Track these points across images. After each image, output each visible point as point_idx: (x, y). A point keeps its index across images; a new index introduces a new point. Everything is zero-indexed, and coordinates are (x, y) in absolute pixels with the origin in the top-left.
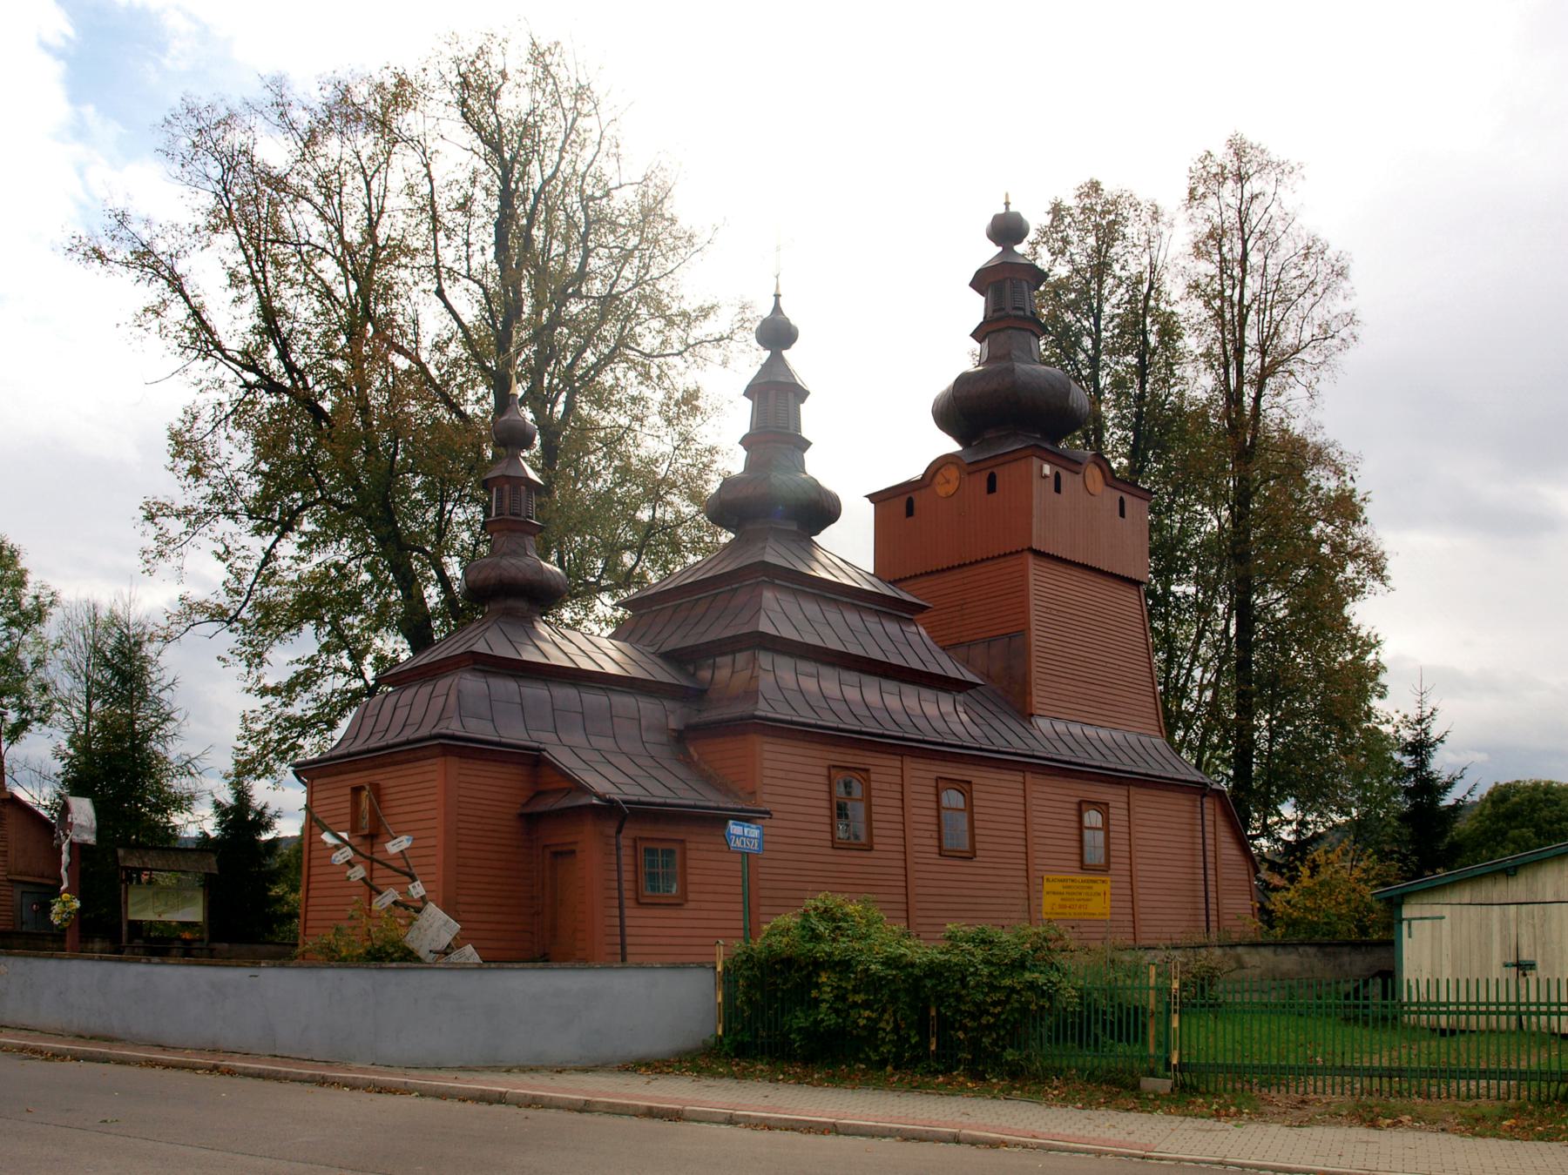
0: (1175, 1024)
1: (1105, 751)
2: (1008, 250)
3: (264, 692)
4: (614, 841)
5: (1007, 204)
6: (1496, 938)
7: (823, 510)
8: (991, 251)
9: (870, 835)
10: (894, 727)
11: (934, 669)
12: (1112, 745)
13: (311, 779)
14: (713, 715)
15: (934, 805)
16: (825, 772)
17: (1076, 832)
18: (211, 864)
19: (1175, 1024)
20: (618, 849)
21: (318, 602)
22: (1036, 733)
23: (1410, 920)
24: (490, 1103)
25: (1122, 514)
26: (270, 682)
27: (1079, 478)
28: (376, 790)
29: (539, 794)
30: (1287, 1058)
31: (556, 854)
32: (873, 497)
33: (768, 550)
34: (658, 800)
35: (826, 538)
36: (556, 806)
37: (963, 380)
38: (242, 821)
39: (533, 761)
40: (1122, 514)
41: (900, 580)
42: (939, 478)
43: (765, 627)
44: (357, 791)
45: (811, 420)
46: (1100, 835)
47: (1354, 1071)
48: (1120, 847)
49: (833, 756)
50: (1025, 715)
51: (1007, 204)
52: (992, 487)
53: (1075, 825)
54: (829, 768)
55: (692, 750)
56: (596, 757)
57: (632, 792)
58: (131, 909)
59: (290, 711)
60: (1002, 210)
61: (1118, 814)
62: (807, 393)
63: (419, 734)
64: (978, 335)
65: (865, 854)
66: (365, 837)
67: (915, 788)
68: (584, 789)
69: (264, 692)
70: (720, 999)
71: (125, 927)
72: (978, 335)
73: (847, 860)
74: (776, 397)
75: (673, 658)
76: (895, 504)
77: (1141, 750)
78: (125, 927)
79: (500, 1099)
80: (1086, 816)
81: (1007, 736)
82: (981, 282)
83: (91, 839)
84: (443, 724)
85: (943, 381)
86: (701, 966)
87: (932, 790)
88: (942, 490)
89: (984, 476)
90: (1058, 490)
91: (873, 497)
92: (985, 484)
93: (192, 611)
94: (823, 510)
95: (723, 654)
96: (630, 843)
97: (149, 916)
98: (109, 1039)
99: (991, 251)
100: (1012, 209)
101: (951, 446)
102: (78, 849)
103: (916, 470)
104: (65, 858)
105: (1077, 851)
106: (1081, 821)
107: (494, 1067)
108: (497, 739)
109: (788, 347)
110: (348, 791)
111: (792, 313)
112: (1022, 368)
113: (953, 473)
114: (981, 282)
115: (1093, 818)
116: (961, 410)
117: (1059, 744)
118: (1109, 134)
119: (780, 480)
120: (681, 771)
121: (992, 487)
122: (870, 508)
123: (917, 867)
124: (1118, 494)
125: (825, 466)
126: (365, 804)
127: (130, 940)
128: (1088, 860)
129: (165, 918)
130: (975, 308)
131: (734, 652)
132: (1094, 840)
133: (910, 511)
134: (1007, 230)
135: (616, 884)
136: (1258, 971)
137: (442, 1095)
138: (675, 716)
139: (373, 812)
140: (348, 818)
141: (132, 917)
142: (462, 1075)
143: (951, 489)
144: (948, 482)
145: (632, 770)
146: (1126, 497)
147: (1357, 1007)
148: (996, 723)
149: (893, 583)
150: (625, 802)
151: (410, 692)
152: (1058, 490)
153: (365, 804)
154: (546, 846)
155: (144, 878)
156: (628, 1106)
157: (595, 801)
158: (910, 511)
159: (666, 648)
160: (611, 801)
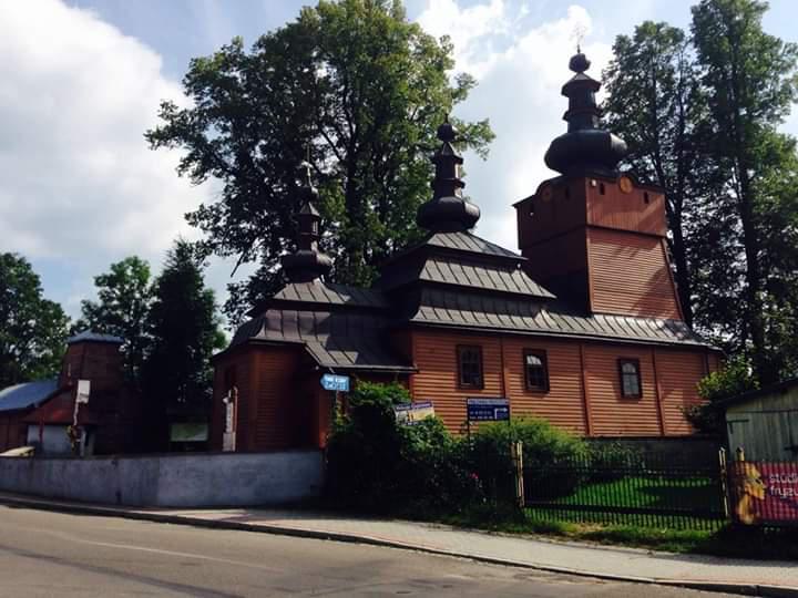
5: (579, 51)
6: (779, 433)
8: (571, 75)
9: (640, 390)
16: (453, 348)
23: (731, 422)
27: (616, 186)
32: (515, 206)
46: (635, 379)
50: (587, 313)
51: (579, 51)
54: (457, 346)
60: (576, 53)
81: (575, 325)
82: (566, 90)
83: (86, 400)
88: (546, 199)
91: (515, 206)
99: (571, 75)
101: (554, 174)
102: (81, 404)
103: (532, 192)
104: (76, 410)
106: (620, 370)
113: (549, 190)
114: (566, 90)
118: (567, 62)
122: (515, 211)
124: (643, 191)
130: (564, 104)
137: (323, 536)
139: (484, 410)
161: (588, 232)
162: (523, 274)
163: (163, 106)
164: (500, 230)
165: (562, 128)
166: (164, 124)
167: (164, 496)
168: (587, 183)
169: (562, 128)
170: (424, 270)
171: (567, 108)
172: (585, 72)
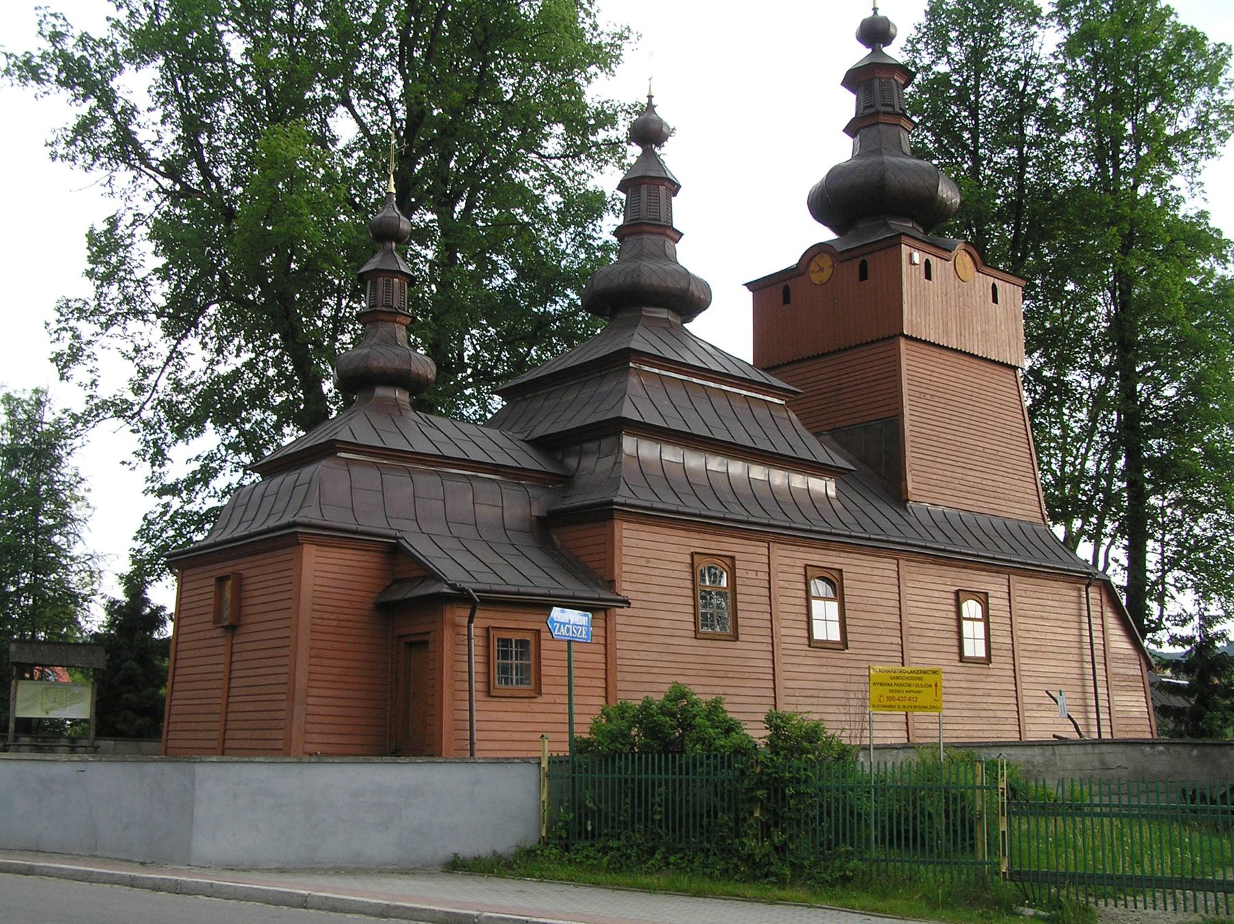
0: (1003, 827)
1: (984, 539)
2: (877, 52)
3: (164, 491)
4: (465, 631)
5: (875, 9)
7: (690, 299)
8: (860, 53)
10: (762, 514)
11: (804, 454)
12: (992, 532)
13: (182, 569)
14: (576, 501)
15: (803, 594)
17: (954, 623)
18: (100, 660)
19: (1003, 827)
20: (469, 639)
21: (218, 403)
22: (912, 520)
24: (292, 907)
25: (995, 300)
26: (169, 480)
28: (239, 580)
29: (398, 582)
30: (1141, 863)
31: (411, 645)
32: (751, 286)
33: (636, 336)
34: (514, 589)
35: (698, 326)
36: (410, 595)
37: (836, 174)
38: (133, 617)
39: (393, 551)
40: (995, 300)
41: (778, 366)
42: (813, 267)
43: (628, 412)
44: (221, 580)
45: (682, 212)
46: (980, 626)
47: (1212, 886)
48: (1001, 638)
49: (696, 543)
51: (875, 9)
52: (863, 275)
53: (953, 615)
54: (692, 555)
55: (555, 537)
56: (453, 544)
57: (487, 581)
58: (19, 706)
59: (193, 507)
61: (998, 603)
62: (679, 187)
63: (284, 521)
64: (851, 129)
65: (730, 644)
66: (226, 628)
67: (782, 576)
68: (433, 576)
69: (164, 491)
70: (544, 797)
71: (12, 725)
72: (851, 129)
73: (712, 652)
74: (650, 191)
75: (543, 445)
76: (771, 293)
77: (1021, 537)
78: (12, 725)
79: (304, 903)
80: (964, 606)
82: (855, 79)
84: (305, 511)
85: (817, 176)
86: (525, 761)
87: (802, 578)
88: (817, 278)
89: (858, 262)
90: (928, 276)
91: (751, 286)
92: (856, 271)
93: (99, 409)
94: (690, 299)
95: (590, 440)
96: (480, 632)
97: (36, 713)
98: (38, 851)
99: (860, 53)
100: (880, 13)
101: (825, 234)
103: (792, 259)
105: (955, 642)
107: (312, 868)
108: (354, 527)
109: (659, 145)
110: (213, 581)
111: (664, 112)
112: (891, 159)
113: (826, 261)
115: (971, 608)
116: (830, 202)
117: (935, 532)
119: (651, 273)
120: (540, 558)
121: (863, 275)
122: (749, 295)
123: (785, 659)
124: (991, 280)
125: (691, 256)
126: (228, 594)
127: (16, 739)
128: (968, 652)
129: (52, 715)
130: (847, 105)
131: (599, 438)
132: (973, 632)
133: (786, 299)
134: (875, 32)
135: (466, 677)
136: (1124, 773)
138: (540, 503)
140: (211, 609)
141: (20, 714)
142: (229, 874)
143: (825, 276)
144: (822, 270)
145: (491, 558)
146: (998, 283)
147: (1214, 812)
148: (869, 509)
149: (766, 370)
150: (475, 591)
151: (278, 480)
152: (928, 276)
153: (228, 594)
154: (400, 636)
155: (37, 673)
156: (371, 905)
157: (446, 590)
158: (786, 299)
159: (539, 432)
160: (463, 590)
161: (902, 342)
162: (793, 416)
163: (54, 159)
164: (727, 328)
165: (842, 150)
166: (38, 46)
167: (203, 846)
168: (905, 257)
169: (842, 150)
170: (627, 401)
171: (851, 114)
172: (886, 50)
